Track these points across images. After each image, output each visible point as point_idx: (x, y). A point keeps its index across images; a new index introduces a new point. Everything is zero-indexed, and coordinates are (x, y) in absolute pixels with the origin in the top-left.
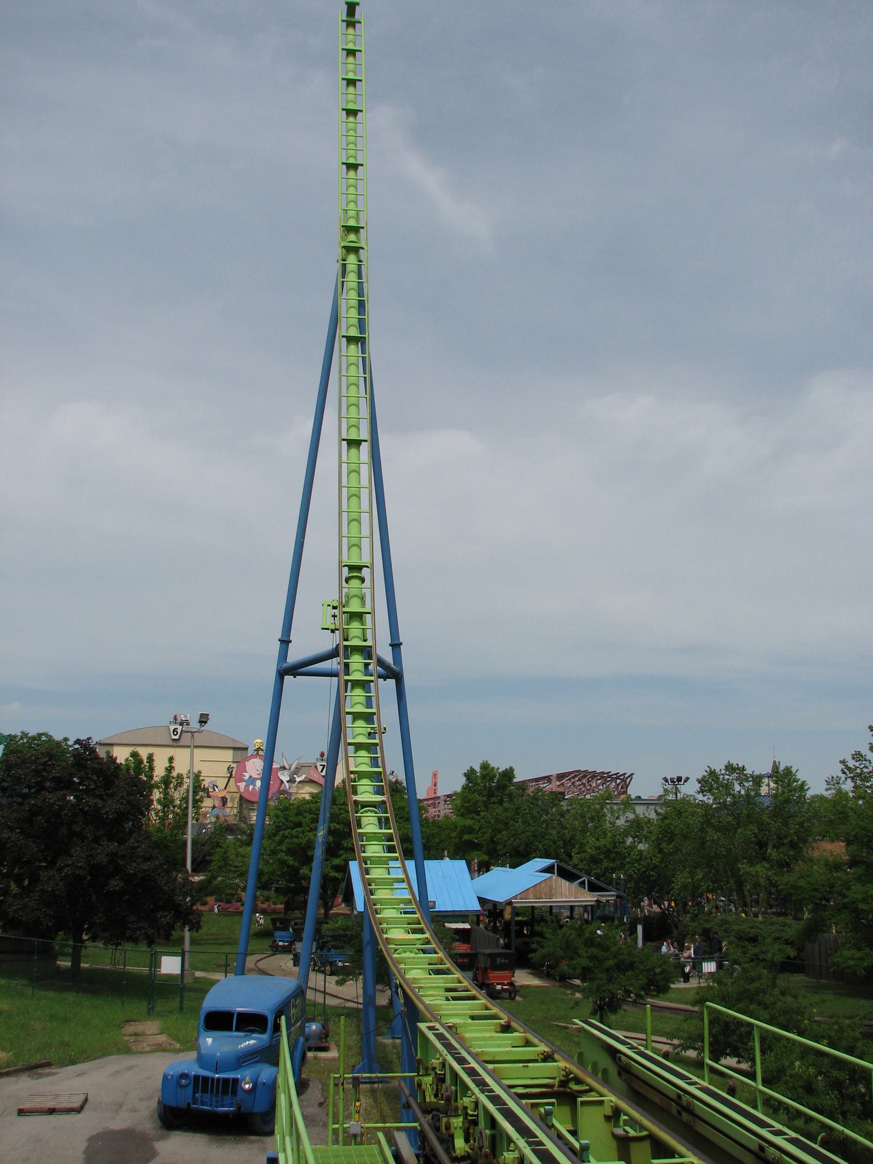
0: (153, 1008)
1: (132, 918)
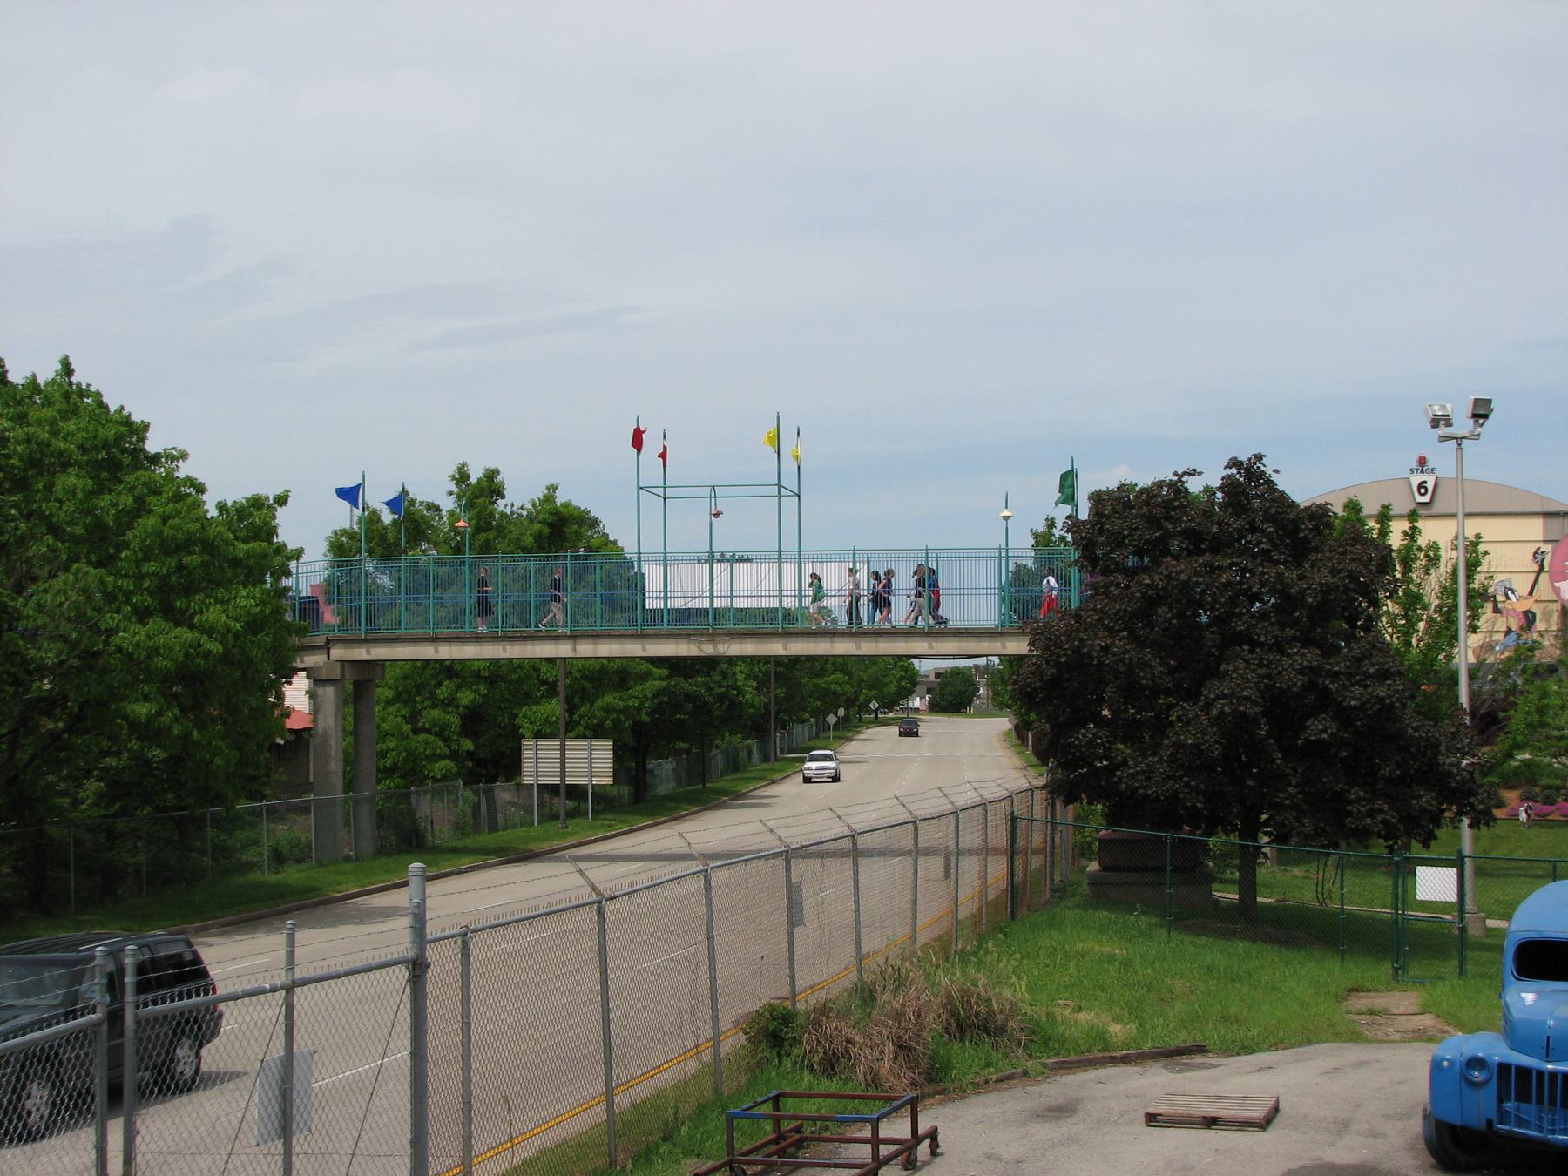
0: (1403, 968)
1: (1357, 792)
